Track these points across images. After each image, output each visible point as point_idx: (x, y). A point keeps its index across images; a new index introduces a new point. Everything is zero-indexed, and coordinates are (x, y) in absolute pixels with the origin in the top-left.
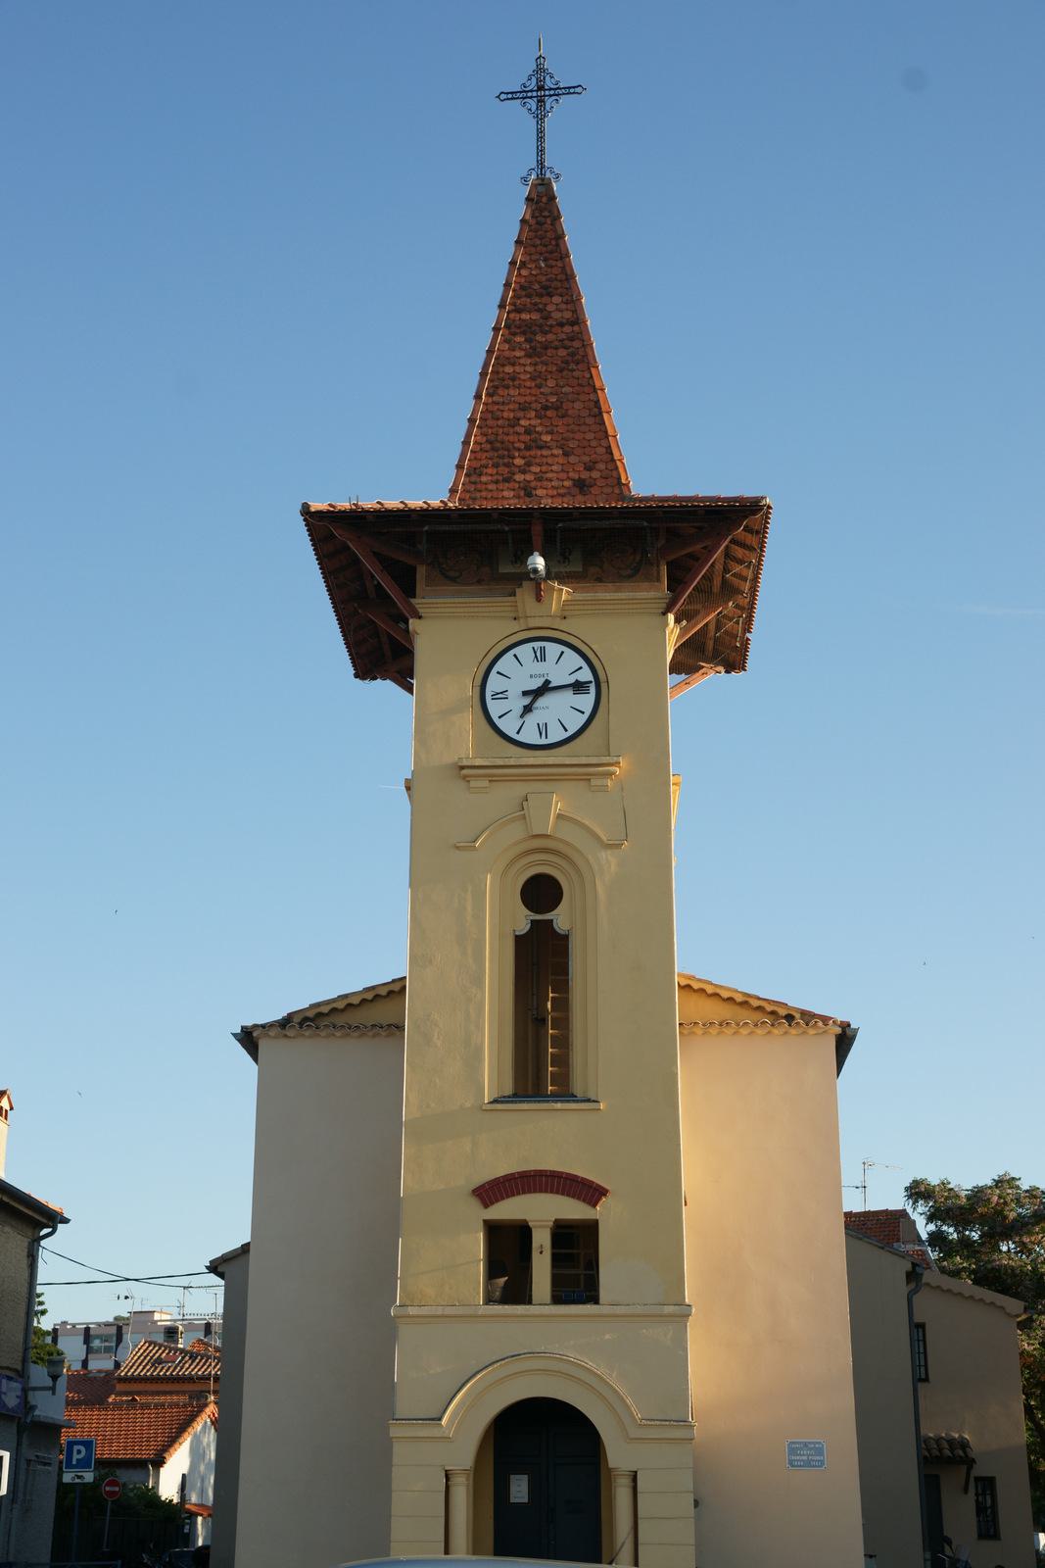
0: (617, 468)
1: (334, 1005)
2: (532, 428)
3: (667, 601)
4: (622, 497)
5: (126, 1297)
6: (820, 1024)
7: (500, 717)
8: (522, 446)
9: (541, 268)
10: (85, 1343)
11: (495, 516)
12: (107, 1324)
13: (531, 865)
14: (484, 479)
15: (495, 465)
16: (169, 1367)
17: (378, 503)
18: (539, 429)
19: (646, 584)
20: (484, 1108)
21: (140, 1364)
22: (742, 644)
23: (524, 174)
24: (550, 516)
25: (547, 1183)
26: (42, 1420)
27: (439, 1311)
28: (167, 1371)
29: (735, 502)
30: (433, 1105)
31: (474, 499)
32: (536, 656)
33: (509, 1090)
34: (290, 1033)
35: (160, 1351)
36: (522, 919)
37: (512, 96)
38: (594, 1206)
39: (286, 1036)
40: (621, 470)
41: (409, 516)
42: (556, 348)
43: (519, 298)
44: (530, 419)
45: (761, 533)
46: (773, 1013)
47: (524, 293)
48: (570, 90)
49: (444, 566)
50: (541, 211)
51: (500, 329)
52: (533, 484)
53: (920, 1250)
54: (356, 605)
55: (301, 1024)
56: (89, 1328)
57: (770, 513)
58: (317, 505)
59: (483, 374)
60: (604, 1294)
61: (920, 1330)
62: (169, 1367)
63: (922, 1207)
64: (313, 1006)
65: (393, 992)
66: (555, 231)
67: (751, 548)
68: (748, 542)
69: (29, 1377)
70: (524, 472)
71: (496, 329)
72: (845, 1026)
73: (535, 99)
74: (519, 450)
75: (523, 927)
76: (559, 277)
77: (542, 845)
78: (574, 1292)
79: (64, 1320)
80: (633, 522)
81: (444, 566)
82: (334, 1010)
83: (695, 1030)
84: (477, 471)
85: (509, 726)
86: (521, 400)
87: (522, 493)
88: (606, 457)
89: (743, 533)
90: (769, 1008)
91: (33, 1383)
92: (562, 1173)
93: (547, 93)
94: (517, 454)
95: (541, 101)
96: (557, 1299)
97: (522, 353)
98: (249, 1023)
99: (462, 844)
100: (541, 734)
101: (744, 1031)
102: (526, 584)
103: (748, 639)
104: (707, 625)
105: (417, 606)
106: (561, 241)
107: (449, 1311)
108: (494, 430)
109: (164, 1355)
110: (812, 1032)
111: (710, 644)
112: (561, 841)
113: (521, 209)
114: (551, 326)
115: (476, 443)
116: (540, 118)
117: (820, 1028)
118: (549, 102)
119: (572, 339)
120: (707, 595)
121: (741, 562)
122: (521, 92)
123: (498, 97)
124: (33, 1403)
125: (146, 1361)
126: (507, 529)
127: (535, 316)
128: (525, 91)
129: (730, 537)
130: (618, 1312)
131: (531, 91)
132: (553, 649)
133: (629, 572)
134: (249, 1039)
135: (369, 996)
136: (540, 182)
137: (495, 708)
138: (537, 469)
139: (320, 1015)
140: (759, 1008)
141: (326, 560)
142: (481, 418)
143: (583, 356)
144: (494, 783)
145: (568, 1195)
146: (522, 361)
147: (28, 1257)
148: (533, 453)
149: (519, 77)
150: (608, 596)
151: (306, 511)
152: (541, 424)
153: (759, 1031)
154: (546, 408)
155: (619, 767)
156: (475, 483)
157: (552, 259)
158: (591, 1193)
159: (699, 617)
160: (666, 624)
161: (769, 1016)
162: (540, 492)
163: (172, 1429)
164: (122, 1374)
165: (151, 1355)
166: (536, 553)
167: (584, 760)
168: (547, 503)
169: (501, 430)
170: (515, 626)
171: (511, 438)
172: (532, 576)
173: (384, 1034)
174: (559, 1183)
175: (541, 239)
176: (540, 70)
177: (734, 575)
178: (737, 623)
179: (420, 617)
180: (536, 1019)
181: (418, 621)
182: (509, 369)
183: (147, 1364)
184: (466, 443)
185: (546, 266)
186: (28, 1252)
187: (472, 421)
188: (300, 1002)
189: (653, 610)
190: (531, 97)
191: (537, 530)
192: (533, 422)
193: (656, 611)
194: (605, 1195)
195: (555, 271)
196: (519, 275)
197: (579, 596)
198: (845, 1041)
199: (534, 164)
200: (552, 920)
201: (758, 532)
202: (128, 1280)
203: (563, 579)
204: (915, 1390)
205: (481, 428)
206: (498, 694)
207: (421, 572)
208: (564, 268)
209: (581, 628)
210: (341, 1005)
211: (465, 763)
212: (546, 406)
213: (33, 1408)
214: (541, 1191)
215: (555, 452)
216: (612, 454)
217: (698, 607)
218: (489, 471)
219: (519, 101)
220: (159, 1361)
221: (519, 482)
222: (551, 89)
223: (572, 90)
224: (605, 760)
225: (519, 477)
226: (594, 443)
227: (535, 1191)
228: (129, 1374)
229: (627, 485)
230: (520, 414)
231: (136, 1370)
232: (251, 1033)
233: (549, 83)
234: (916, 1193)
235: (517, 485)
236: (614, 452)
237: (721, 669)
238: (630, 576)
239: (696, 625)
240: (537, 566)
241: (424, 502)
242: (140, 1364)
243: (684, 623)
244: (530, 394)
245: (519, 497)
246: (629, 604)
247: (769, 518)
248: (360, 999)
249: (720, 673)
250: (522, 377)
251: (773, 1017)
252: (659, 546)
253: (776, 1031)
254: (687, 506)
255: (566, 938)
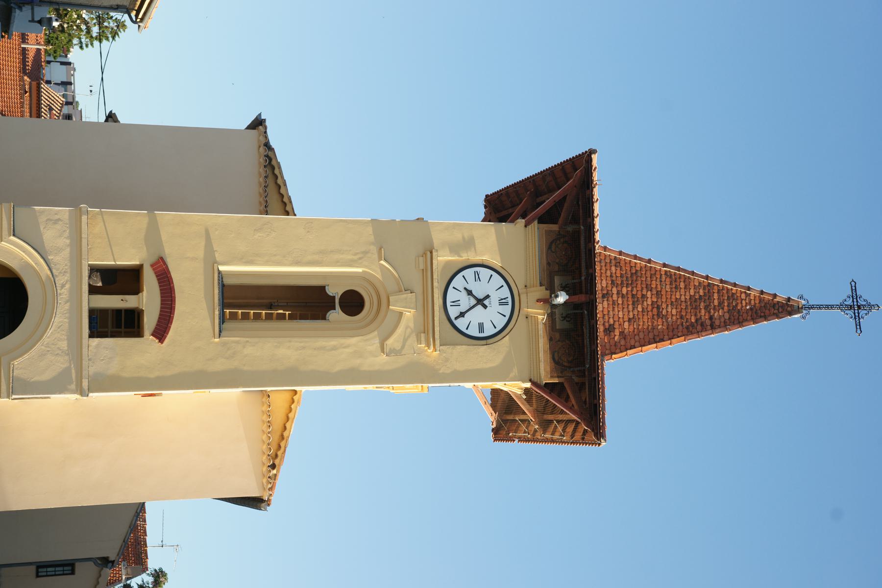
0: (621, 352)
1: (279, 177)
2: (646, 299)
3: (539, 382)
4: (603, 355)
5: (91, 91)
6: (270, 486)
7: (463, 276)
8: (634, 293)
9: (746, 306)
10: (61, 82)
11: (591, 271)
12: (74, 97)
13: (370, 296)
14: (613, 268)
15: (622, 276)
16: (47, 115)
17: (597, 200)
18: (645, 303)
19: (549, 369)
20: (215, 265)
21: (49, 97)
22: (510, 437)
23: (805, 297)
24: (592, 306)
25: (167, 304)
26: (13, 14)
27: (84, 236)
28: (44, 113)
29: (602, 422)
30: (217, 233)
31: (600, 262)
32: (502, 299)
33: (227, 281)
34: (262, 149)
35: (57, 110)
36: (335, 291)
37: (854, 289)
38: (153, 335)
39: (260, 147)
40: (620, 355)
41: (590, 217)
42: (696, 315)
43: (727, 293)
44: (651, 298)
45: (583, 441)
46: (276, 456)
47: (730, 295)
48: (858, 326)
49: (558, 242)
50: (782, 307)
51: (707, 280)
52: (610, 299)
53: (122, 579)
54: (532, 190)
55: (267, 156)
56: (71, 85)
57: (596, 446)
58: (595, 157)
59: (678, 269)
60: (96, 341)
61: (70, 572)
62: (47, 115)
63: (150, 579)
64: (279, 164)
65: (286, 208)
66: (769, 316)
67: (572, 436)
68: (576, 434)
69: (40, 6)
70: (618, 294)
71: (707, 277)
72: (268, 502)
73: (852, 304)
74: (632, 291)
75: (330, 291)
76: (740, 317)
77: (382, 303)
78: (96, 323)
79: (76, 70)
80: (589, 358)
81: (558, 242)
82: (276, 177)
83: (266, 406)
84: (618, 264)
85: (458, 282)
86: (663, 293)
87: (605, 292)
88: (628, 346)
89: (583, 429)
90: (279, 453)
91: (36, 9)
92: (173, 283)
93: (856, 311)
94: (629, 289)
95: (851, 307)
96: (92, 312)
97: (692, 294)
98: (267, 123)
99: (383, 252)
100: (453, 302)
101: (264, 437)
102: (548, 292)
103: (514, 441)
104: (524, 413)
105: (533, 224)
106: (763, 319)
107: (84, 242)
108: (644, 275)
109: (54, 112)
110: (265, 481)
111: (510, 417)
112: (385, 316)
113: (782, 295)
114: (709, 312)
115: (636, 263)
116: (840, 307)
117: (267, 485)
118: (851, 312)
119: (702, 325)
120: (544, 411)
121: (564, 430)
122: (856, 295)
123: (853, 281)
124: (24, 9)
125: (51, 101)
126: (583, 278)
127: (716, 303)
128: (857, 297)
129: (580, 421)
130: (84, 350)
131: (857, 301)
132: (507, 310)
133: (556, 358)
134: (258, 123)
135: (285, 200)
136: (800, 306)
137: (469, 273)
138: (620, 301)
139: (273, 168)
140: (280, 447)
141: (561, 168)
142: (651, 267)
143: (691, 332)
144: (422, 271)
145: (159, 318)
146: (687, 293)
147: (117, 5)
148: (630, 299)
149: (866, 293)
150: (541, 345)
151: (592, 152)
152: (648, 305)
153: (265, 447)
154: (658, 307)
155: (433, 352)
156: (610, 262)
157: (752, 313)
158: (161, 333)
159: (528, 406)
160: (524, 381)
161: (274, 454)
162: (605, 303)
163: (11, 75)
164: (42, 86)
165: (55, 104)
166: (567, 297)
167: (437, 329)
168: (600, 308)
169: (644, 279)
170: (521, 286)
171: (639, 286)
172: (553, 295)
173: (262, 208)
174: (166, 312)
175: (764, 306)
176: (871, 307)
177: (556, 427)
178: (525, 432)
179: (526, 226)
180: (272, 305)
181: (524, 225)
182: (682, 285)
183: (49, 101)
184: (635, 257)
185: (747, 310)
186: (120, 5)
187: (649, 261)
188: (282, 156)
189: (532, 373)
190: (853, 301)
191: (582, 298)
192: (649, 300)
193: (532, 375)
194: (160, 341)
195: (745, 315)
196: (741, 293)
197: (541, 327)
198: (255, 502)
199: (811, 303)
200: (335, 309)
201: (583, 439)
202: (102, 74)
203: (551, 316)
204: (30, 564)
205: (645, 267)
206: (478, 275)
207: (555, 227)
208: (746, 320)
209: (520, 327)
210: (279, 181)
211: (434, 254)
212: (660, 309)
213: (20, 8)
214: (162, 301)
215: (631, 314)
216: (630, 349)
217: (535, 405)
218: (618, 272)
219: (851, 294)
220: (51, 109)
221: (611, 290)
222: (859, 313)
223: (858, 327)
224: (438, 342)
225: (615, 290)
226: (637, 338)
227: (162, 297)
228: (42, 90)
229: (611, 358)
230: (654, 292)
231: (45, 94)
232: (261, 125)
233: (862, 312)
234: (159, 575)
235: (610, 289)
236: (632, 350)
237: (494, 426)
238: (553, 358)
239: (523, 404)
240: (560, 297)
241: (598, 229)
242: (49, 97)
243: (524, 397)
244: (667, 298)
245: (602, 290)
246: (536, 358)
247: (592, 445)
248: (283, 193)
249: (492, 425)
250: (678, 293)
251: (274, 456)
252: (573, 378)
253: (265, 457)
254: (599, 392)
255: (324, 318)
